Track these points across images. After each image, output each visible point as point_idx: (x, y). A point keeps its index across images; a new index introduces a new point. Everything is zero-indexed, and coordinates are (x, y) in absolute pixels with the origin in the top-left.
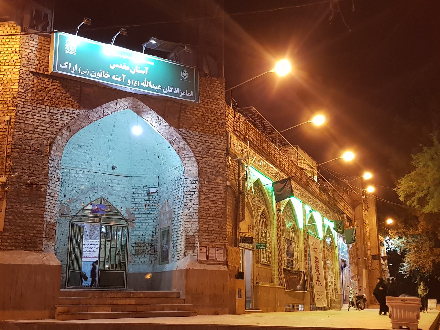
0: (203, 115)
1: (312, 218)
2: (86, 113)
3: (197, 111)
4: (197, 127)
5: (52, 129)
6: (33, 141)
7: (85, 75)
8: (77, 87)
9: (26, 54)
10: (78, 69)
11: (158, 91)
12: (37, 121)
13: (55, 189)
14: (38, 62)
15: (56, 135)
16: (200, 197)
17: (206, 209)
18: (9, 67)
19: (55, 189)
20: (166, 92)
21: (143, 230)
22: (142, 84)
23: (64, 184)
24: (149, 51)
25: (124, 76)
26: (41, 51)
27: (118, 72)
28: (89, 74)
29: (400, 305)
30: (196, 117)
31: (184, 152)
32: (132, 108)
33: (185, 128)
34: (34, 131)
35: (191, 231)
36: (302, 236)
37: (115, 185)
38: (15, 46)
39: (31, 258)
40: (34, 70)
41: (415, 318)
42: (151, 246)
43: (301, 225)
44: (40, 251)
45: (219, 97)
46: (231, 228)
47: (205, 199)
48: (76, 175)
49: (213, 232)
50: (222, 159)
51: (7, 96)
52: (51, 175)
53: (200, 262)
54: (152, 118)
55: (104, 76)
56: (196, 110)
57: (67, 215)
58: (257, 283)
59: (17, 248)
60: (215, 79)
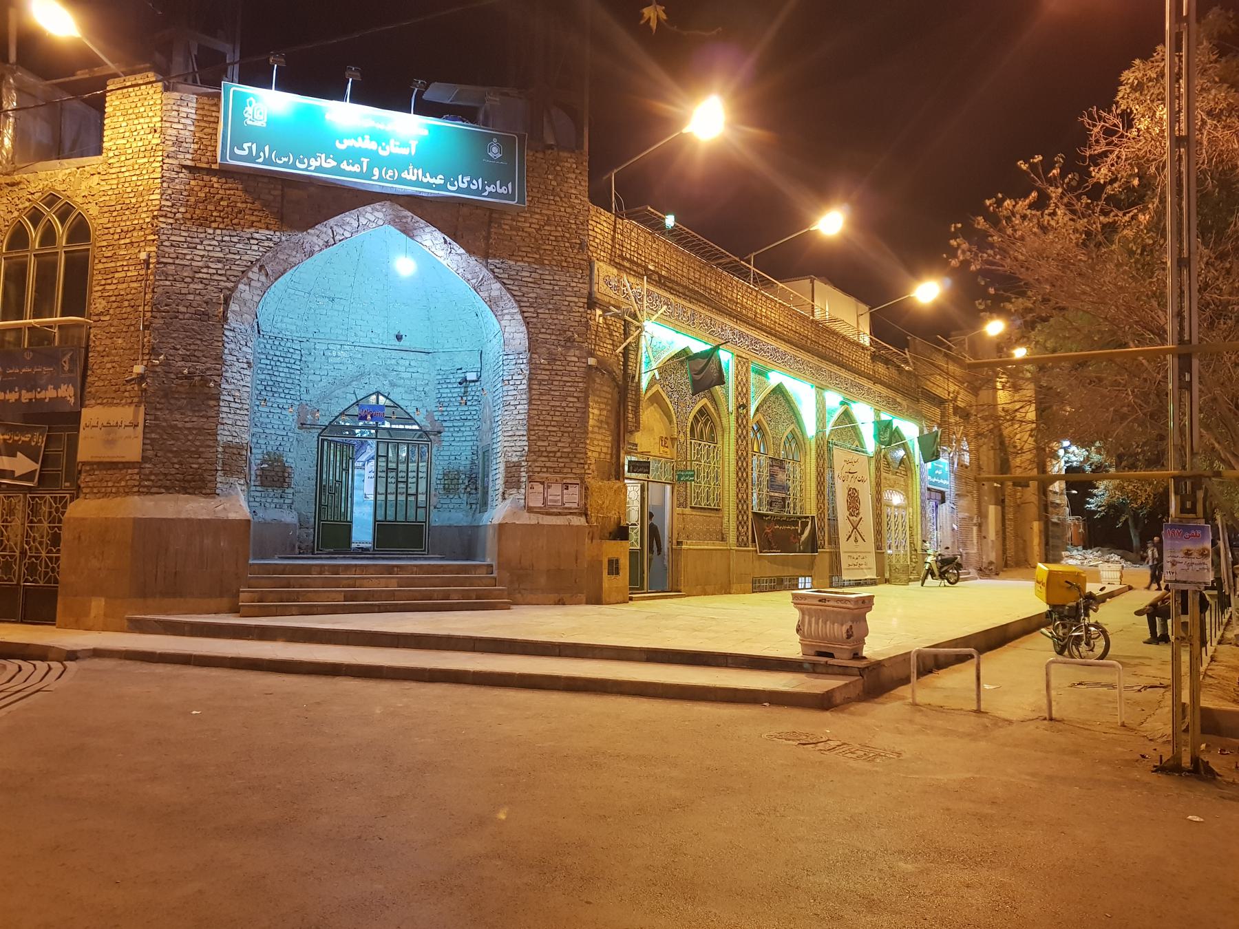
0: (538, 230)
1: (846, 416)
2: (295, 239)
5: (229, 273)
6: (191, 297)
7: (285, 165)
8: (275, 189)
9: (175, 132)
11: (438, 187)
12: (199, 258)
13: (242, 383)
14: (196, 146)
15: (237, 283)
16: (530, 388)
18: (146, 160)
19: (242, 383)
21: (454, 451)
23: (306, 370)
24: (425, 109)
25: (365, 161)
26: (203, 124)
27: (354, 155)
28: (294, 162)
29: (816, 610)
31: (502, 304)
32: (393, 222)
33: (500, 257)
34: (193, 278)
36: (813, 452)
37: (403, 369)
38: (155, 119)
39: (194, 508)
40: (189, 163)
41: (845, 636)
42: (470, 479)
43: (811, 430)
44: (213, 494)
45: (573, 191)
47: (541, 394)
48: (328, 353)
49: (559, 454)
51: (144, 215)
52: (230, 358)
53: (530, 510)
54: (432, 240)
55: (324, 165)
57: (313, 426)
58: (679, 543)
59: (169, 490)
60: (566, 154)
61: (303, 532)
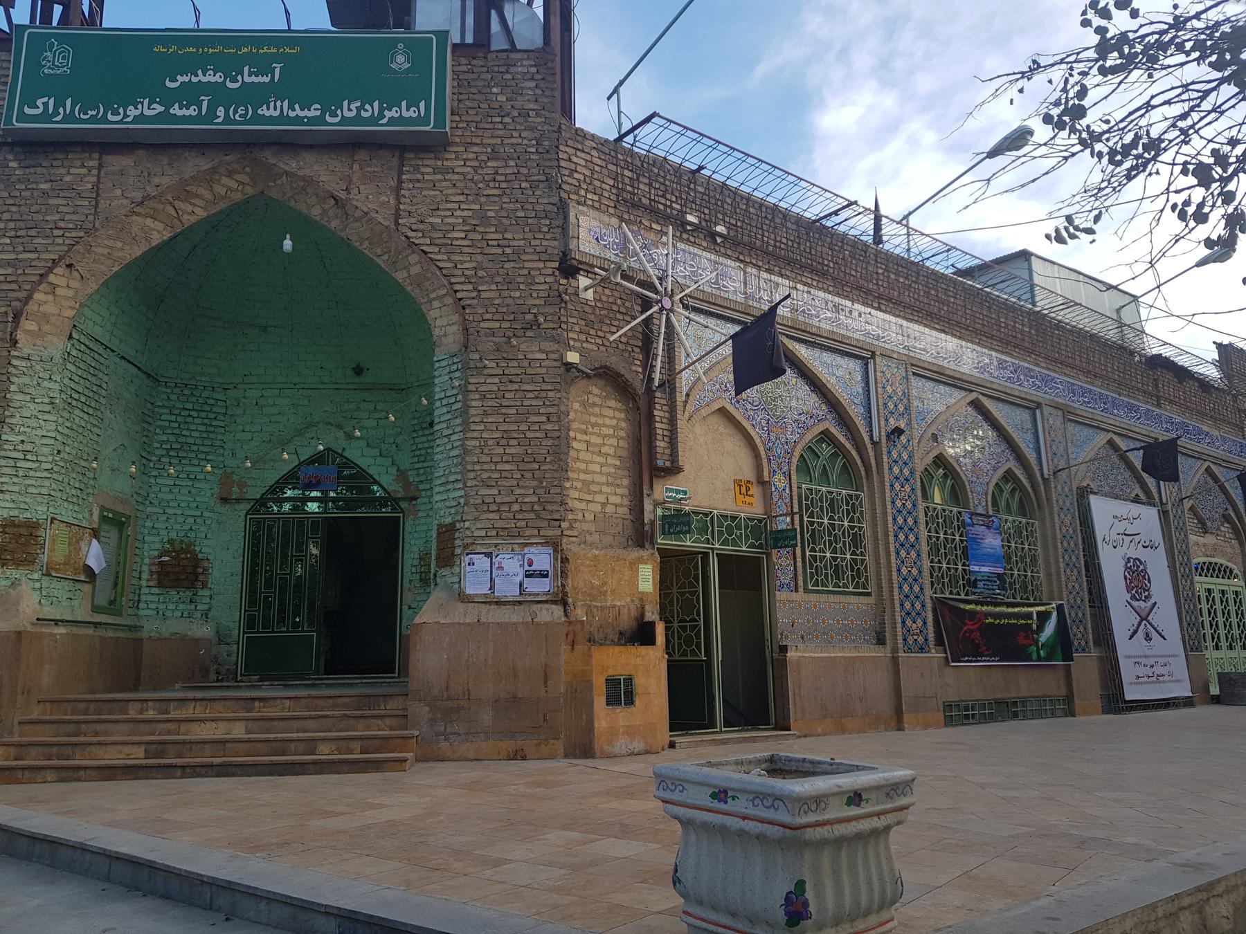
3: (456, 159)
4: (456, 206)
5: (21, 279)
7: (93, 120)
10: (72, 109)
11: (312, 121)
13: (39, 432)
17: (490, 442)
19: (39, 432)
20: (337, 120)
22: (259, 112)
28: (105, 113)
30: (456, 177)
35: (447, 511)
46: (626, 491)
47: (486, 414)
49: (516, 507)
50: (547, 287)
55: (147, 112)
56: (453, 156)
61: (223, 649)
